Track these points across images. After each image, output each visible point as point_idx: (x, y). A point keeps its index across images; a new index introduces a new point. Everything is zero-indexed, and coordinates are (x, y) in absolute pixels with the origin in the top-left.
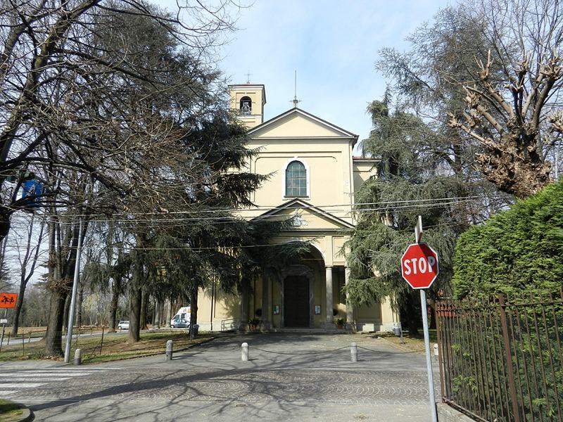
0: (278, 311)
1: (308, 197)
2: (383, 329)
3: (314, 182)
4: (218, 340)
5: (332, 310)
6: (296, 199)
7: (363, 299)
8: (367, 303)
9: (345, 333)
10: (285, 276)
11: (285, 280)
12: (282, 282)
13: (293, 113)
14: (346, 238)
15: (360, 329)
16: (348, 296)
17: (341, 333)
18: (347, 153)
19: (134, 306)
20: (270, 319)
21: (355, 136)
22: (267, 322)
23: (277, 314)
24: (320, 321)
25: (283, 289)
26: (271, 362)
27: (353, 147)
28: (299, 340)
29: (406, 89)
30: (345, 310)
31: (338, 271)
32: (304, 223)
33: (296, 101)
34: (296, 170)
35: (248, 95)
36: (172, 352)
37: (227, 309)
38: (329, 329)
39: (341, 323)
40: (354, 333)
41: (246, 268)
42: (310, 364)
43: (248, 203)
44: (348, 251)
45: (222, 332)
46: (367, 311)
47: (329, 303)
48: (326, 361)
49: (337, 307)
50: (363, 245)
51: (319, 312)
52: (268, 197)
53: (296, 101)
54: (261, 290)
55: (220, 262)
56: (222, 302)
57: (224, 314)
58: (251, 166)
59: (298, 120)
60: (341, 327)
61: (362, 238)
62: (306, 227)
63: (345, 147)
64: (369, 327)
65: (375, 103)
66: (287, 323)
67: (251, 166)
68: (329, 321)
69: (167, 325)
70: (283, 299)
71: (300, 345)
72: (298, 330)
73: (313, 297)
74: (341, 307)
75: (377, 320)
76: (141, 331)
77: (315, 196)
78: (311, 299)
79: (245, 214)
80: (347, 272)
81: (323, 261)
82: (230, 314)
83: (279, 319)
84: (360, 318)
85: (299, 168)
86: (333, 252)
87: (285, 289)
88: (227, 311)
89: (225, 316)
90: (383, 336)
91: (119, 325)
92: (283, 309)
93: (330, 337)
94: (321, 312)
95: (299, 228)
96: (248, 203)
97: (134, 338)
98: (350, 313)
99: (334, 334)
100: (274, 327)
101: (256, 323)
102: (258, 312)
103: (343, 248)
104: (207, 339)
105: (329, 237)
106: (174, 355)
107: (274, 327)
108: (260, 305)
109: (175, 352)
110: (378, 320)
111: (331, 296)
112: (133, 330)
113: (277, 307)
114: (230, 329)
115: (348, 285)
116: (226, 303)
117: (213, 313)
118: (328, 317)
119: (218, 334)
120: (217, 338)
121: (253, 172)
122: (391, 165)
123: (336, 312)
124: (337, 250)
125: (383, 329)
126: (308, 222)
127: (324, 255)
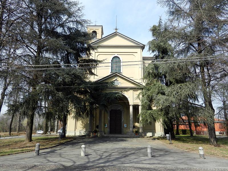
0: (106, 126)
1: (121, 73)
2: (157, 135)
3: (124, 64)
4: (75, 141)
5: (132, 126)
6: (116, 74)
7: (149, 120)
8: (150, 123)
9: (139, 137)
10: (110, 110)
11: (110, 111)
12: (109, 113)
13: (115, 34)
14: (139, 91)
15: (146, 135)
16: (140, 119)
17: (137, 137)
18: (139, 54)
19: (29, 123)
20: (103, 130)
21: (144, 45)
22: (101, 131)
23: (106, 128)
24: (127, 131)
25: (109, 116)
26: (99, 157)
27: (143, 51)
28: (117, 141)
29: (172, 13)
30: (138, 126)
31: (136, 107)
32: (119, 84)
33: (116, 29)
34: (116, 60)
35: (95, 30)
36: (40, 149)
37: (82, 125)
38: (131, 135)
39: (137, 132)
40: (143, 137)
41: (91, 104)
42: (123, 160)
43: (92, 74)
44: (141, 96)
45: (79, 136)
46: (150, 127)
47: (131, 122)
48: (133, 157)
49: (134, 125)
50: (149, 93)
51: (126, 127)
52: (101, 72)
53: (116, 29)
54: (99, 116)
55: (77, 102)
56: (80, 122)
57: (81, 127)
58: (94, 55)
59: (117, 38)
60: (137, 134)
61: (148, 90)
62: (120, 86)
63: (139, 50)
64: (149, 134)
65: (154, 26)
66: (111, 132)
67: (94, 55)
68: (131, 131)
69: (55, 132)
70: (109, 121)
71: (117, 144)
72: (116, 135)
73: (123, 120)
74: (137, 124)
75: (153, 131)
76: (33, 135)
77: (125, 71)
78: (122, 121)
79: (93, 79)
80: (140, 108)
81: (128, 102)
82: (84, 127)
83: (107, 130)
84: (145, 131)
85: (118, 59)
86: (133, 98)
87: (110, 115)
88: (83, 126)
89: (82, 128)
90: (158, 138)
91: (37, 132)
92: (109, 125)
93: (132, 139)
94: (128, 126)
95: (118, 86)
96: (92, 74)
97: (29, 140)
98: (141, 127)
99: (134, 137)
100: (105, 134)
101: (96, 132)
102: (97, 127)
103: (139, 95)
104: (69, 140)
105: (131, 91)
106: (41, 151)
107: (105, 134)
108: (98, 124)
109: (42, 149)
110: (154, 131)
111: (132, 119)
112: (28, 135)
113: (106, 124)
114: (83, 135)
115: (141, 113)
116: (82, 122)
117: (75, 127)
118: (131, 129)
119: (77, 137)
120: (75, 139)
121: (96, 59)
122: (163, 52)
123: (134, 127)
124: (136, 96)
125: (157, 135)
126: (120, 83)
127: (129, 99)
